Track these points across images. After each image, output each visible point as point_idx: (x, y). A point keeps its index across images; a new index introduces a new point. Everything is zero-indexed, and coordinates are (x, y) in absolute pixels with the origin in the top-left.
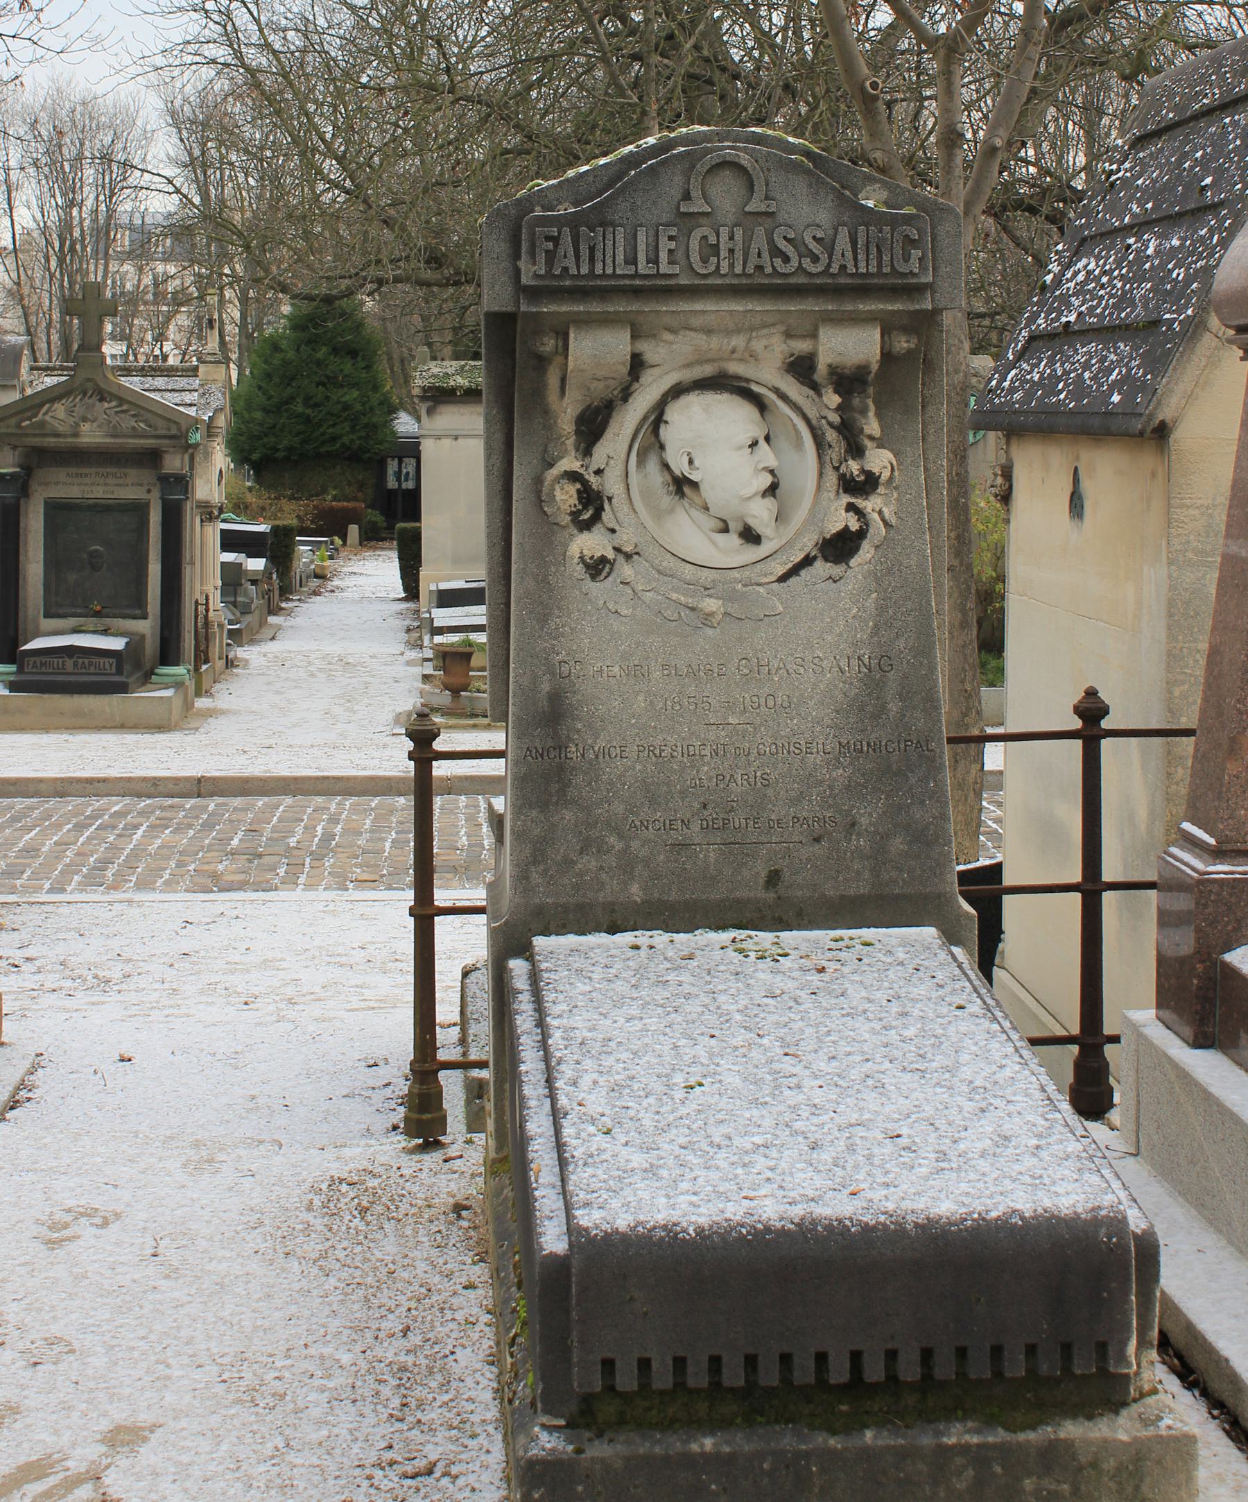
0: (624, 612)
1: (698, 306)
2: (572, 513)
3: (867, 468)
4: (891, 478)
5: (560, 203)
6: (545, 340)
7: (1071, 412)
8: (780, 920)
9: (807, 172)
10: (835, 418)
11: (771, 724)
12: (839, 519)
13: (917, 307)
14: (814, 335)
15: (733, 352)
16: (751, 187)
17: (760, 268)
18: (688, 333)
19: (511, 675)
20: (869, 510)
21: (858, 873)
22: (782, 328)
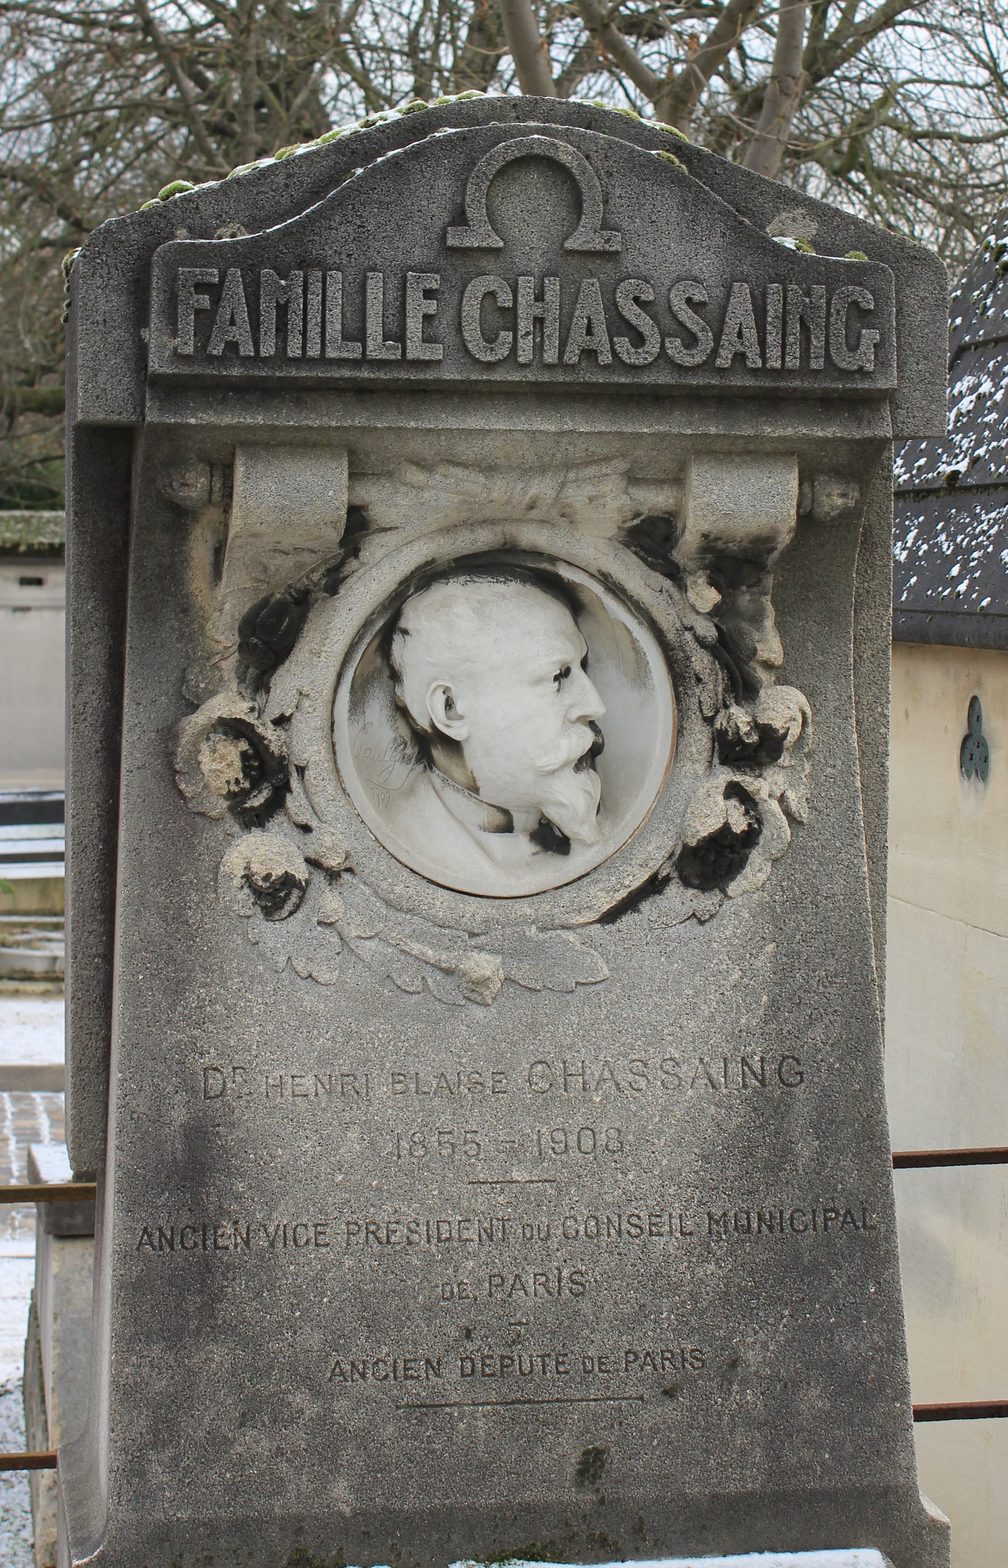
0: (324, 977)
1: (474, 422)
2: (231, 795)
3: (762, 720)
4: (801, 738)
5: (224, 223)
6: (190, 477)
7: (985, 613)
8: (604, 1541)
9: (678, 180)
10: (707, 630)
11: (588, 1181)
12: (713, 813)
13: (868, 433)
14: (678, 480)
15: (531, 507)
16: (577, 207)
17: (590, 354)
18: (452, 470)
19: (114, 1092)
20: (764, 794)
21: (743, 1452)
22: (623, 466)
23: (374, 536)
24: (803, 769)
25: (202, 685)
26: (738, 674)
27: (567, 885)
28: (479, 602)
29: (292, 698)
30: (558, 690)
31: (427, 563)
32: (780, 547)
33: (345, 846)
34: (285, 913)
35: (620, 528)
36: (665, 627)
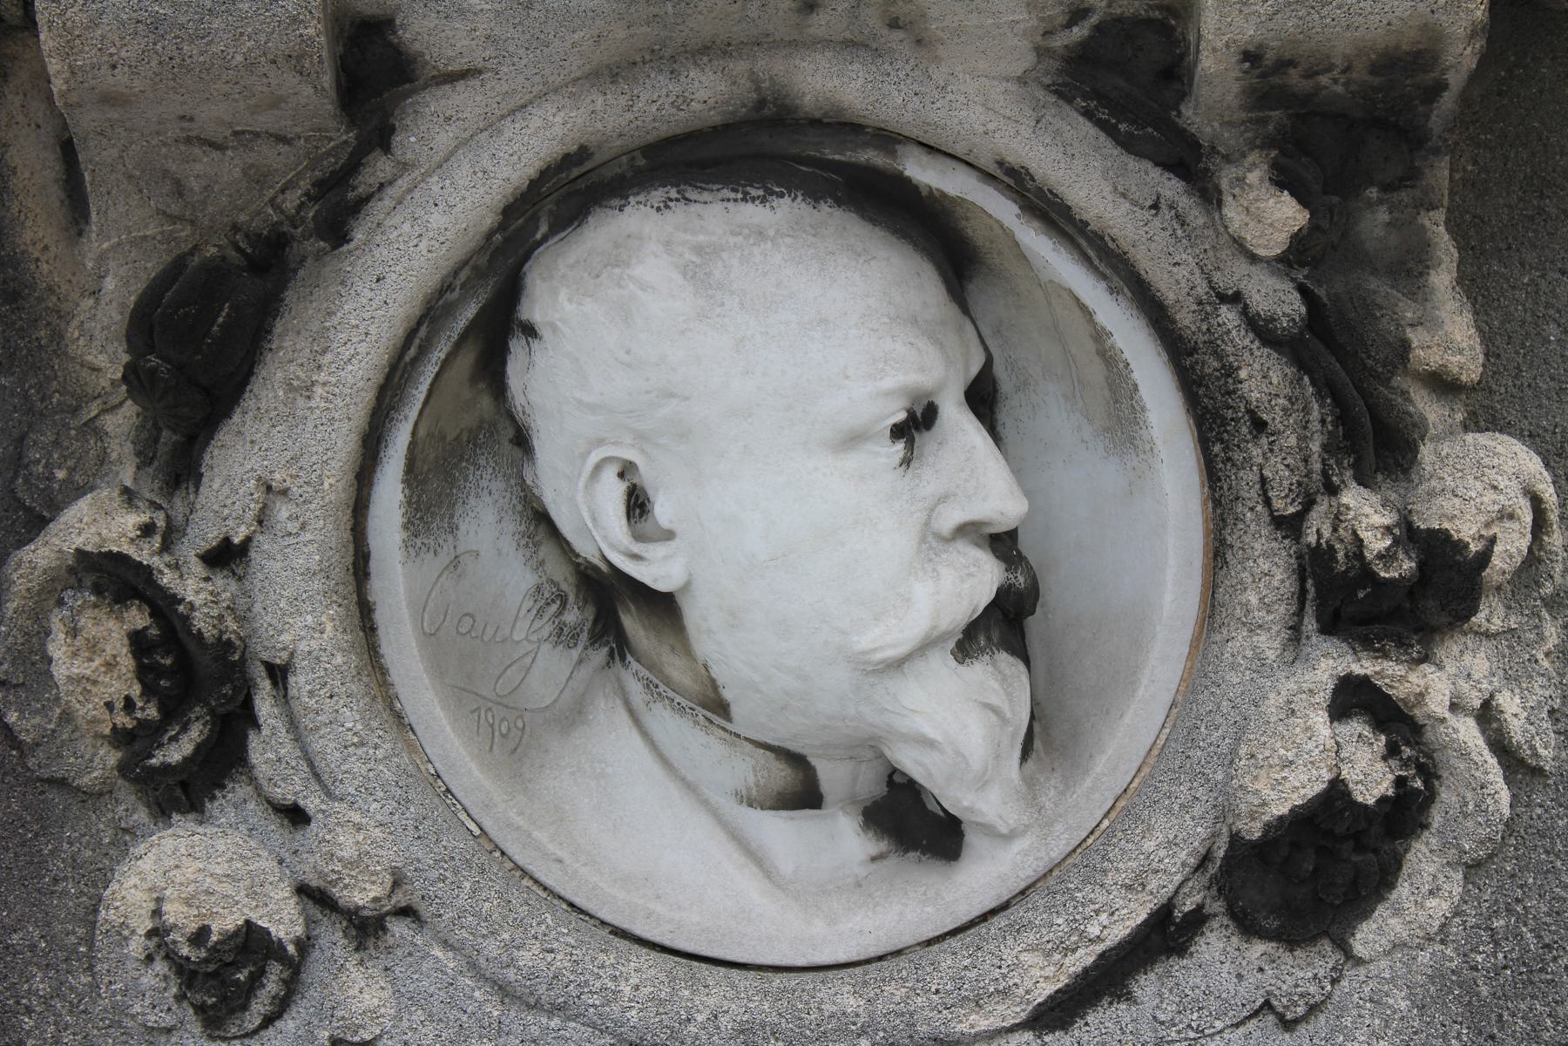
2: (120, 738)
3: (1428, 519)
4: (1533, 560)
10: (1278, 299)
12: (1302, 752)
20: (1437, 704)
23: (427, 96)
24: (1541, 638)
25: (61, 474)
26: (1360, 407)
27: (953, 933)
28: (699, 250)
29: (246, 499)
30: (906, 462)
31: (568, 161)
32: (1456, 80)
33: (389, 855)
34: (252, 1019)
35: (1041, 52)
36: (1170, 297)
